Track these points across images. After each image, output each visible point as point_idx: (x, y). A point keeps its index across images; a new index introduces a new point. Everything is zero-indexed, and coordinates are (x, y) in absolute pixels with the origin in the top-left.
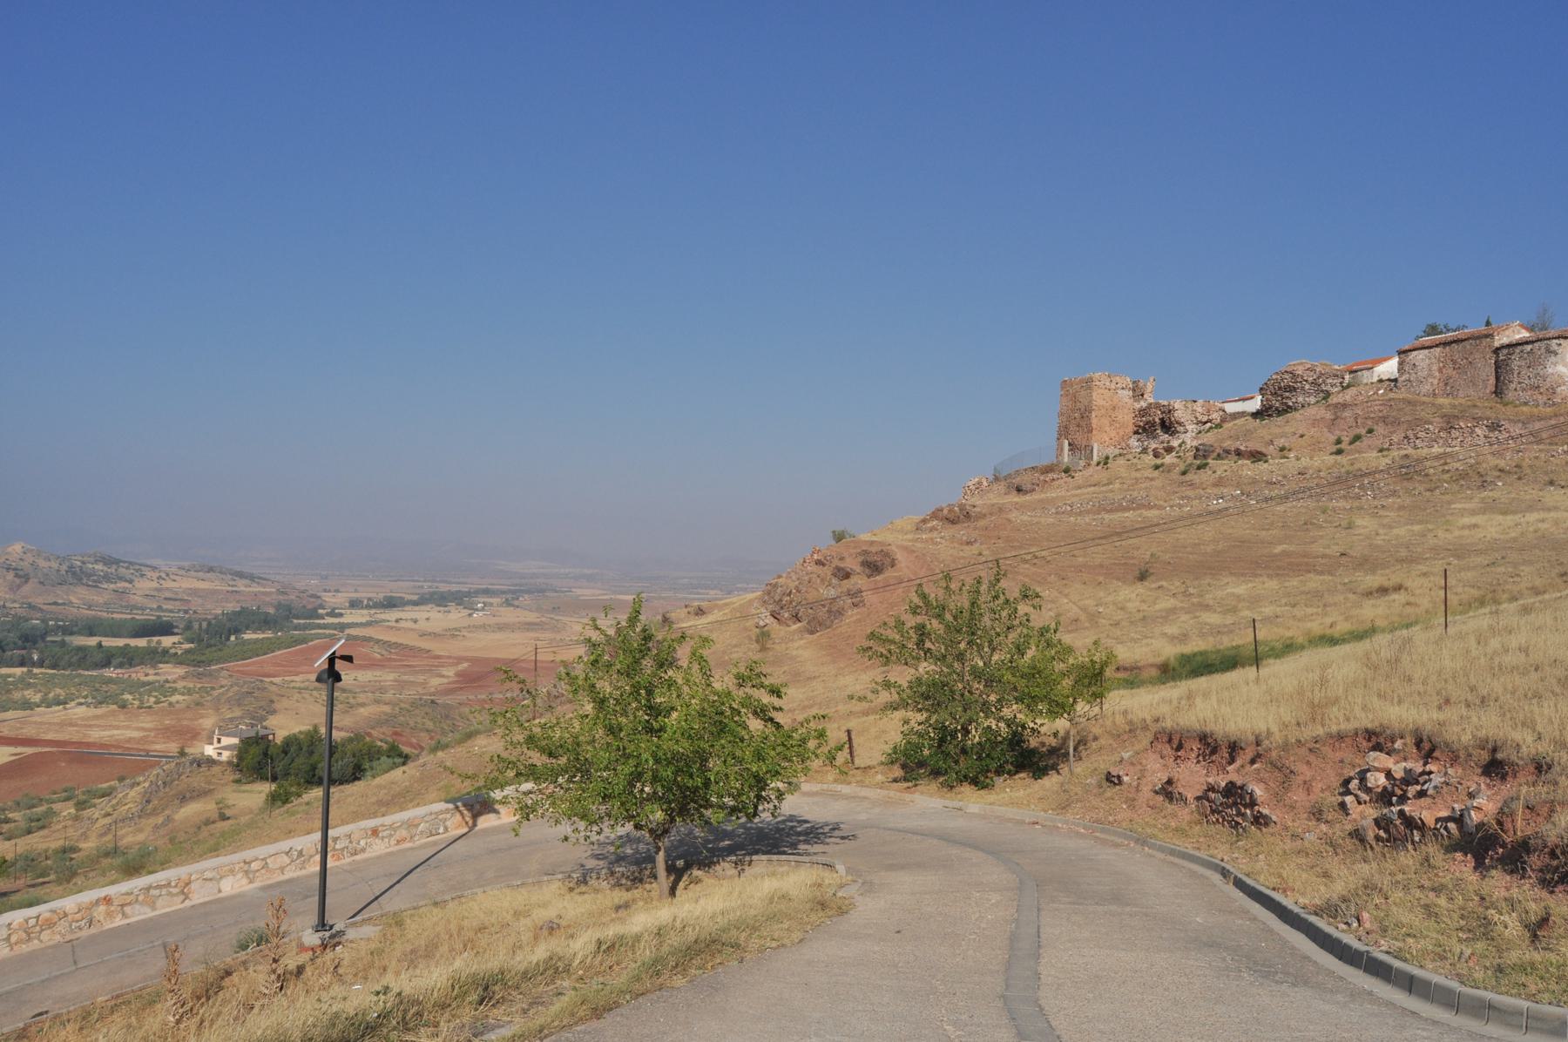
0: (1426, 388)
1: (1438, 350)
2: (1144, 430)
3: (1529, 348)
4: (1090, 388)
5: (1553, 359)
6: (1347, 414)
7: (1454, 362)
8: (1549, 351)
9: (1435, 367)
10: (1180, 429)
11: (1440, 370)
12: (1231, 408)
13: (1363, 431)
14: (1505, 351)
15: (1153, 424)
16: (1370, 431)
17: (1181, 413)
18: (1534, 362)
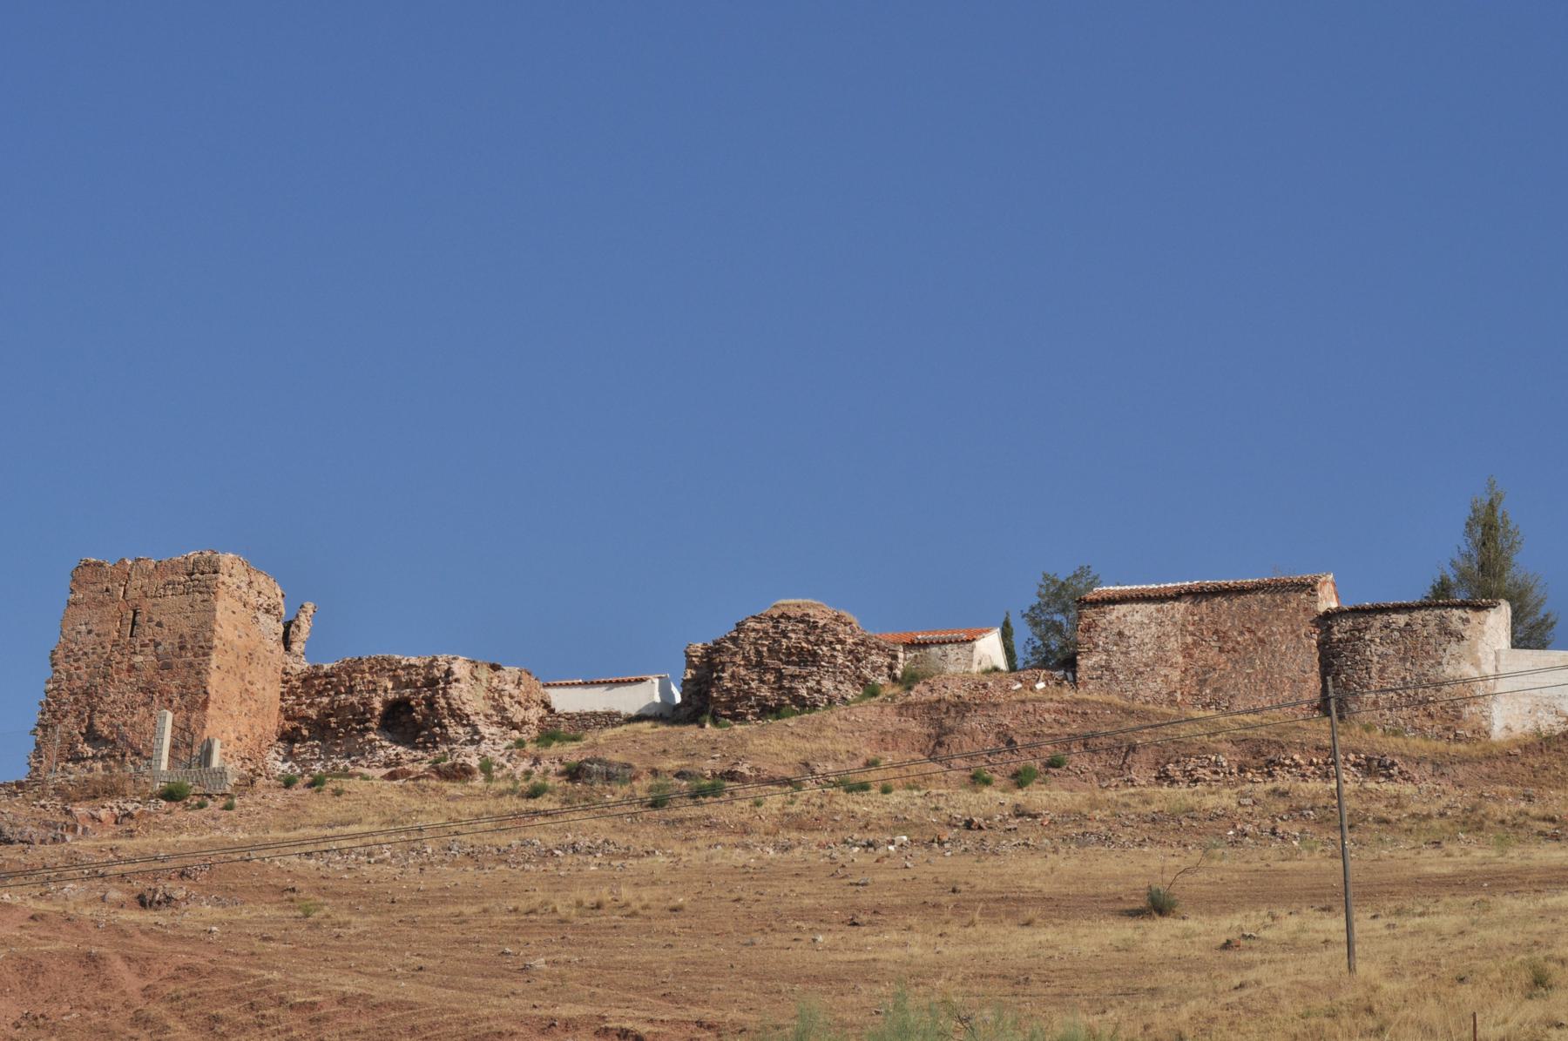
0: (1152, 686)
1: (1181, 606)
2: (321, 729)
3: (1401, 619)
4: (209, 591)
5: (1453, 647)
6: (974, 722)
7: (1222, 636)
8: (1446, 631)
9: (1173, 644)
10: (455, 730)
11: (1187, 652)
12: (567, 701)
13: (1037, 765)
14: (1347, 624)
15: (361, 716)
16: (1054, 763)
17: (468, 693)
18: (1413, 649)
